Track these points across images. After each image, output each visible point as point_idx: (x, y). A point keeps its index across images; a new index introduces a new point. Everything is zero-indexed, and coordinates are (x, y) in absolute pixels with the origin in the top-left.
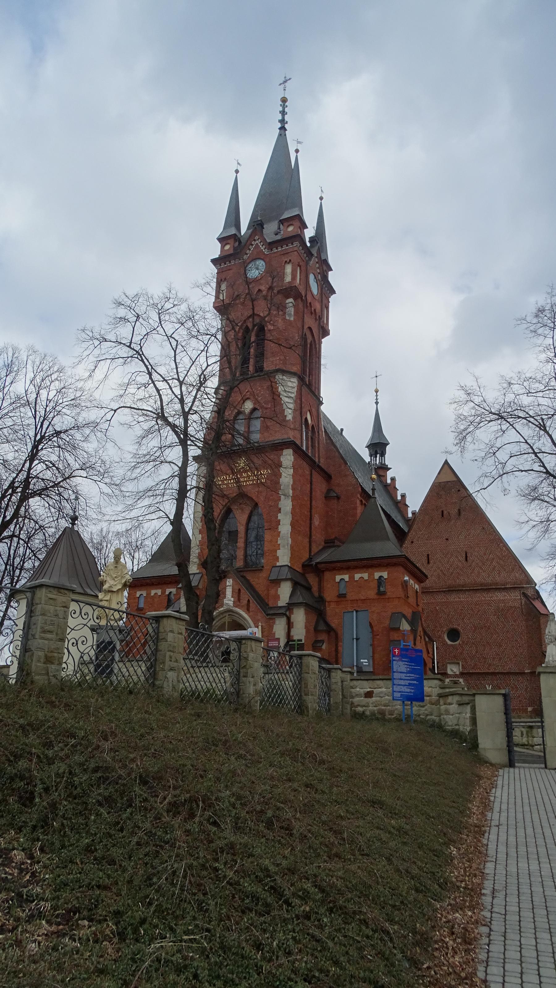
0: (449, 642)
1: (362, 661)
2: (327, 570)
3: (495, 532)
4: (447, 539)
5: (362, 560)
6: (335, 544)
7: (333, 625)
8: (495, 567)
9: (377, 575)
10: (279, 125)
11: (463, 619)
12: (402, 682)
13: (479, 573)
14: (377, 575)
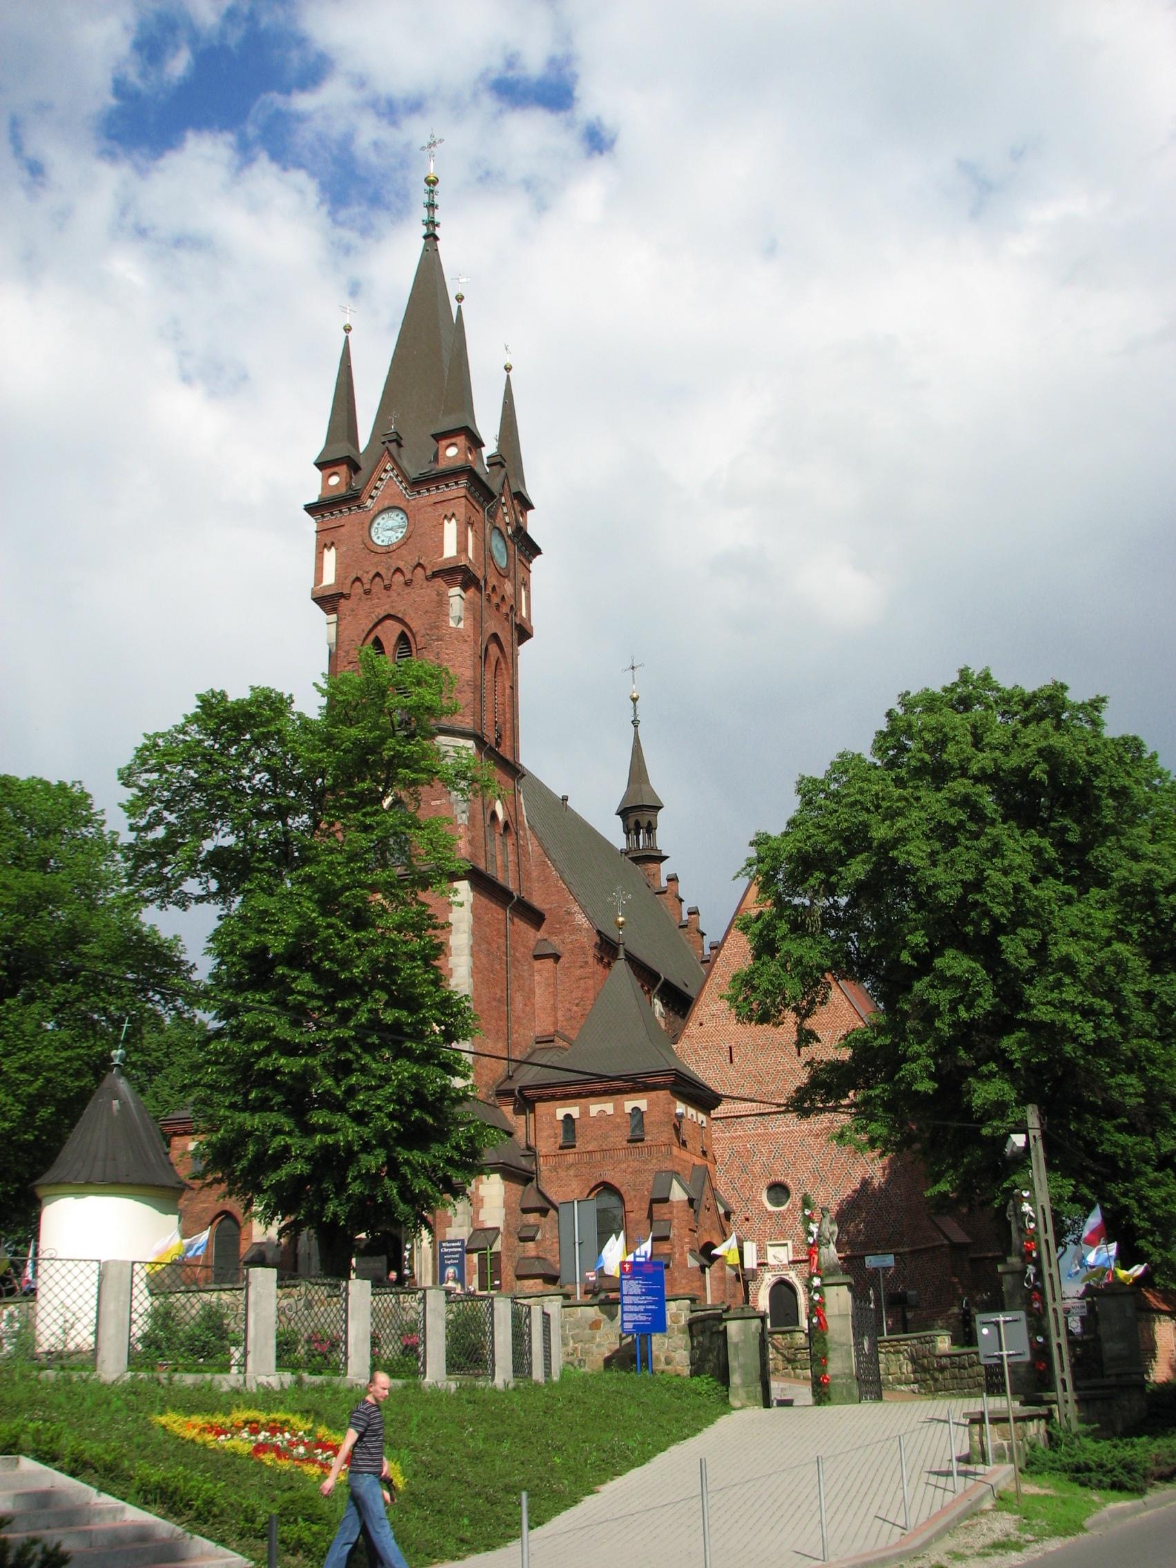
0: (771, 1208)
2: (541, 1099)
9: (629, 1106)
10: (424, 230)
12: (636, 1309)
14: (629, 1106)
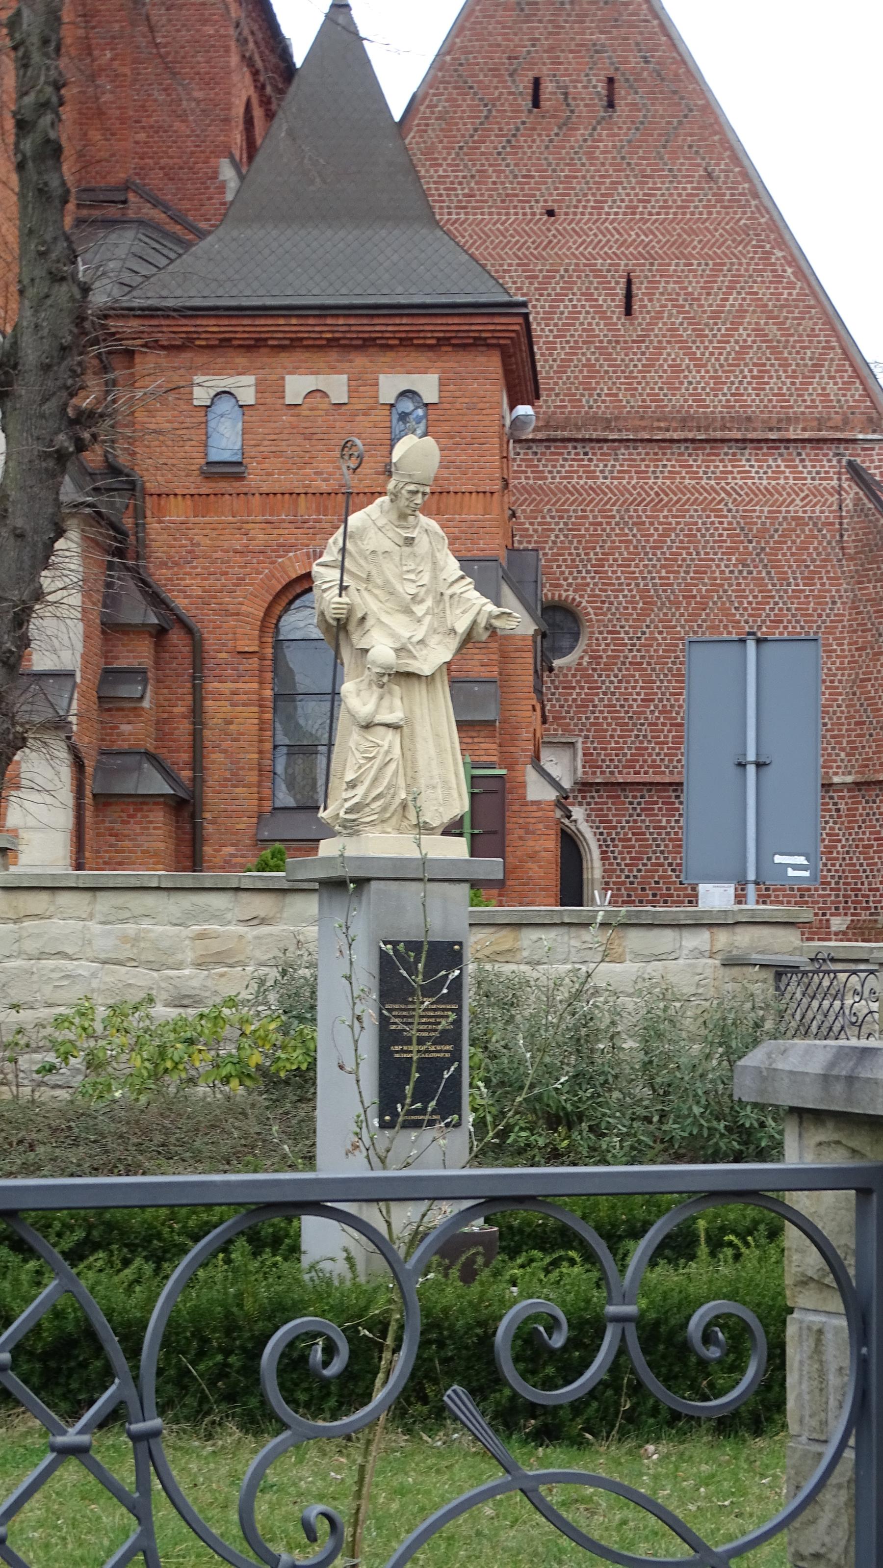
1: (778, 859)
3: (756, 195)
4: (551, 213)
5: (324, 311)
6: (131, 214)
7: (181, 603)
8: (745, 348)
11: (601, 563)
13: (676, 369)
